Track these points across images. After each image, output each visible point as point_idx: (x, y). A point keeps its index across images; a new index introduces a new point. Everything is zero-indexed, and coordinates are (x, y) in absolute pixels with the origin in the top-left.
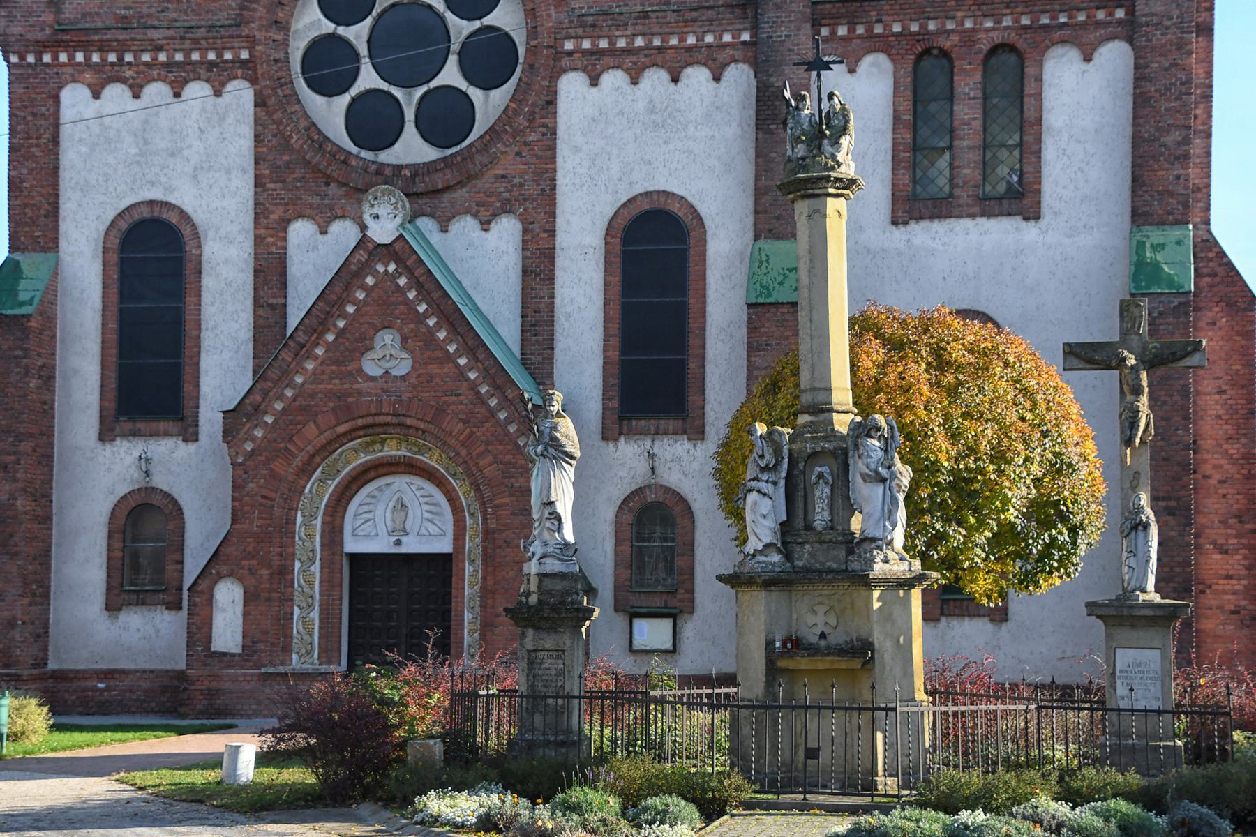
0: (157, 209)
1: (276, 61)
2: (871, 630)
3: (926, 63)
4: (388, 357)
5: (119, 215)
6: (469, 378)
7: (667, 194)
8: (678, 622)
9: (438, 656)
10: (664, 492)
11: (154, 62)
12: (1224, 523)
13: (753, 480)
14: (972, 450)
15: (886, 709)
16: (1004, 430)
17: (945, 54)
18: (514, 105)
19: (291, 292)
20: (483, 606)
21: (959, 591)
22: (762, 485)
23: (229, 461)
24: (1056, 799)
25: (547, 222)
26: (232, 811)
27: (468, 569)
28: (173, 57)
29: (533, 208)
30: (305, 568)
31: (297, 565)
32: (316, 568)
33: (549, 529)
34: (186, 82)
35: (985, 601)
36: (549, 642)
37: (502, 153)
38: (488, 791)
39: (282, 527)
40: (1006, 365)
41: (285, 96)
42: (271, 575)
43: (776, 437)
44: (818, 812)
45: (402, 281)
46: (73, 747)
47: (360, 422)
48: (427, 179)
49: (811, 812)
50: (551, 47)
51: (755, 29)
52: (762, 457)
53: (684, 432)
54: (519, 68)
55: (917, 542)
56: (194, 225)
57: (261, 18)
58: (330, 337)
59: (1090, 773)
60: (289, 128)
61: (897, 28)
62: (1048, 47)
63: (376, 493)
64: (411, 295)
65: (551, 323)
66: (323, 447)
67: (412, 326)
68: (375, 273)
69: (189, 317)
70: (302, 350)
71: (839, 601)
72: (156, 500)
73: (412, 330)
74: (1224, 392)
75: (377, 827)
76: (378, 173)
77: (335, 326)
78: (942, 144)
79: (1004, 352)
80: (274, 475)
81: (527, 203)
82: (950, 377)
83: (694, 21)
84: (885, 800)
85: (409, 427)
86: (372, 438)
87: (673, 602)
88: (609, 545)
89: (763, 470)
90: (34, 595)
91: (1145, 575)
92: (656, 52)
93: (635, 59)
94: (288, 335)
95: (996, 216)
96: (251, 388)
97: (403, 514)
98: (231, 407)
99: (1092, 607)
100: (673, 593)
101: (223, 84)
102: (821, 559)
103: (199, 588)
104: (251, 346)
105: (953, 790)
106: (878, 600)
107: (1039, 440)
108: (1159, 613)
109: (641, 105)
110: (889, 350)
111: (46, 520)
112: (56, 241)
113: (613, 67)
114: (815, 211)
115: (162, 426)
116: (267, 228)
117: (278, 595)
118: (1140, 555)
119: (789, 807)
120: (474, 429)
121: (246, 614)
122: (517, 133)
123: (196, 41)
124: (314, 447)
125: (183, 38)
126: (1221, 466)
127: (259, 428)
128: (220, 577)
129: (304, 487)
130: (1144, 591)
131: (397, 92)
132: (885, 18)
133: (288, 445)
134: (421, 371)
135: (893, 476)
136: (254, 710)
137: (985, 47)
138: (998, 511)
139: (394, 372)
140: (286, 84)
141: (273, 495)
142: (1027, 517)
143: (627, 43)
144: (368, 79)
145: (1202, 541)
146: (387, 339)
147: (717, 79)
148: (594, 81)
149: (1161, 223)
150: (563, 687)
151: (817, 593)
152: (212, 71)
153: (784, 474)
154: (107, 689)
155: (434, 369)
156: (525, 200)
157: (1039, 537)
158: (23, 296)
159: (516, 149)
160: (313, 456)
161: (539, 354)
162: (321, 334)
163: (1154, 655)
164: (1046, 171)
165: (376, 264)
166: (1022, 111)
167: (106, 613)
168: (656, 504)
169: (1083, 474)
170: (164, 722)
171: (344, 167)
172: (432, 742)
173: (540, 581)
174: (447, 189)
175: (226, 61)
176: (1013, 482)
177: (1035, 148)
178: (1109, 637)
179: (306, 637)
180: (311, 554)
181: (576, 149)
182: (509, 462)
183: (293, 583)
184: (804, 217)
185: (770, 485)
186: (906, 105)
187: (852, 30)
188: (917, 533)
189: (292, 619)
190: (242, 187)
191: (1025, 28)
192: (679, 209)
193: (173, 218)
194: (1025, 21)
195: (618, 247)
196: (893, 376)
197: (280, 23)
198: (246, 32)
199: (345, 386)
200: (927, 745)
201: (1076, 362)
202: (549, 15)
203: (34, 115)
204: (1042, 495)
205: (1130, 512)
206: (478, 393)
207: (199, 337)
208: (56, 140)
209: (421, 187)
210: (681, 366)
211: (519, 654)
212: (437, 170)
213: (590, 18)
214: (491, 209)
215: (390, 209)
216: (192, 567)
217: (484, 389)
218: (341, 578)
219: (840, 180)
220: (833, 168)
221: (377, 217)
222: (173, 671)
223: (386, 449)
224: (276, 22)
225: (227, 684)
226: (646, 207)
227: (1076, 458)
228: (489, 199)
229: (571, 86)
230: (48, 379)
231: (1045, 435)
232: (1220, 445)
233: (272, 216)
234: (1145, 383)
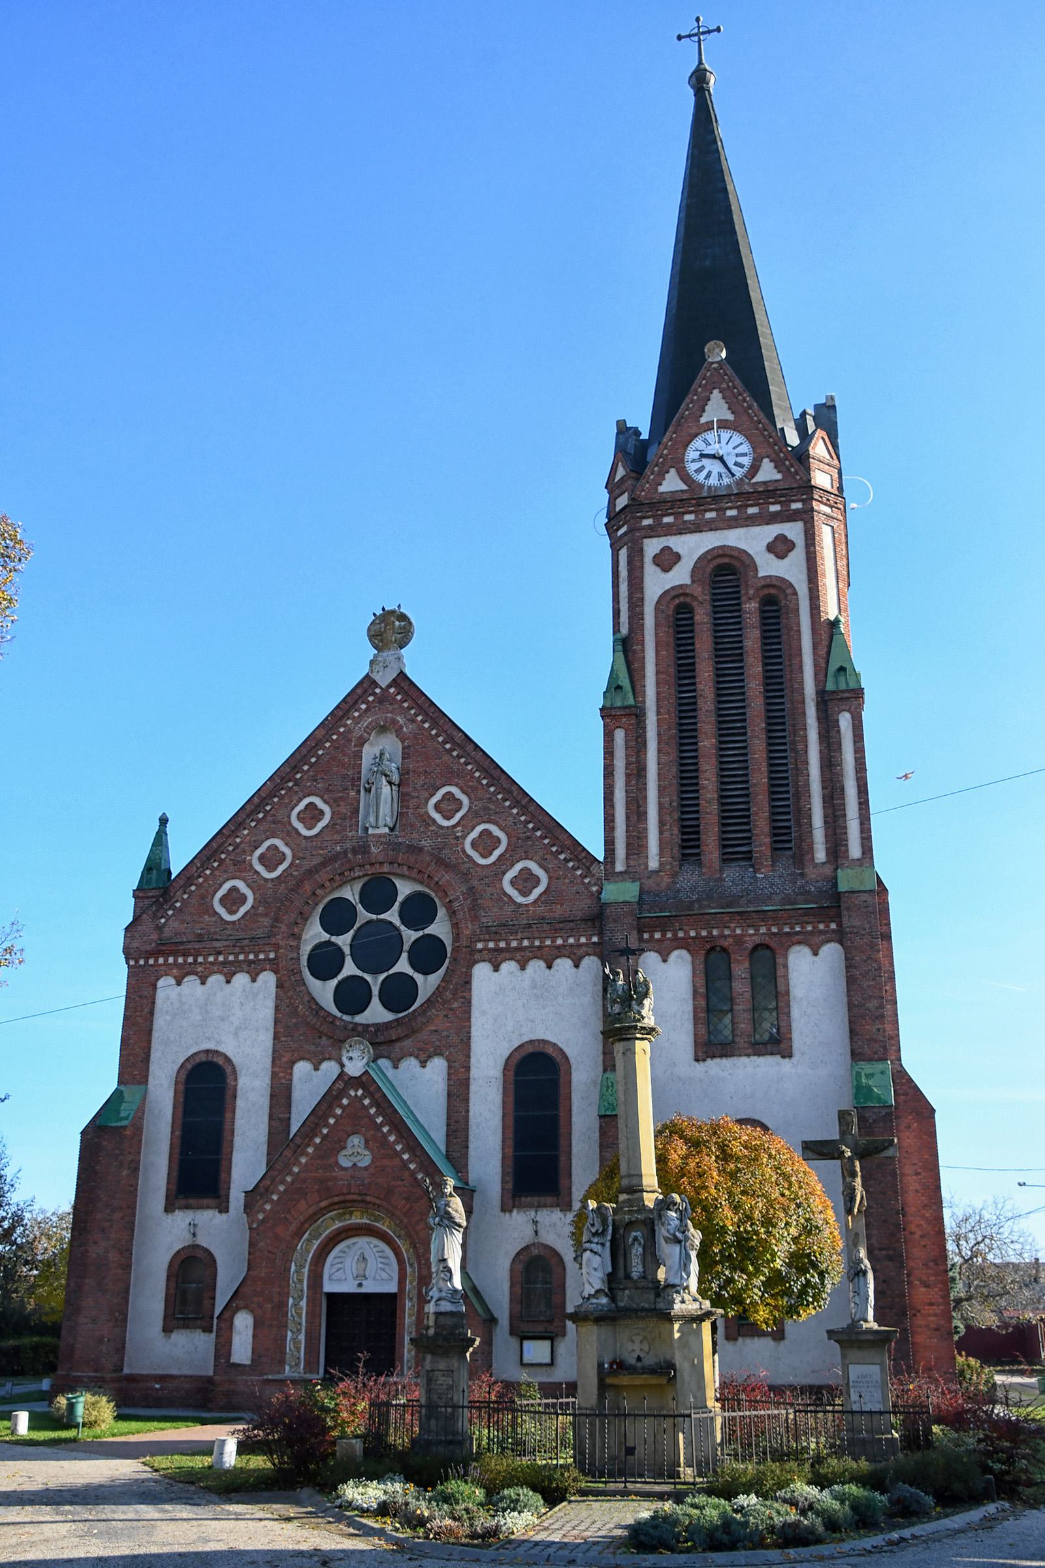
0: (210, 1055)
1: (292, 959)
2: (674, 1353)
3: (713, 955)
5: (187, 1059)
9: (366, 1374)
12: (925, 1265)
13: (588, 1242)
14: (749, 1218)
15: (684, 1416)
16: (770, 1203)
17: (724, 950)
19: (294, 1109)
21: (746, 1318)
22: (593, 1246)
23: (247, 1226)
24: (809, 1483)
26: (212, 1492)
27: (408, 1304)
31: (291, 1301)
32: (303, 1303)
33: (443, 1279)
34: (235, 973)
35: (764, 1326)
36: (442, 1365)
37: (436, 1016)
38: (393, 1480)
40: (770, 1156)
43: (603, 1211)
44: (634, 1498)
46: (128, 1433)
47: (336, 1199)
49: (630, 1498)
51: (601, 934)
52: (593, 1225)
53: (558, 1206)
54: (447, 961)
55: (713, 1285)
58: (318, 1140)
59: (833, 1462)
61: (692, 933)
62: (790, 946)
63: (346, 1250)
64: (373, 1111)
65: (466, 1130)
66: (311, 1217)
69: (227, 1127)
70: (299, 1150)
71: (651, 1332)
72: (199, 1254)
74: (919, 1173)
75: (309, 1509)
76: (353, 1029)
77: (321, 1132)
78: (726, 1008)
79: (768, 1148)
82: (732, 1166)
83: (561, 929)
84: (685, 1487)
85: (370, 1202)
88: (506, 1286)
89: (594, 1234)
90: (117, 1320)
91: (867, 1309)
93: (523, 954)
94: (291, 1136)
95: (763, 1055)
97: (363, 1265)
98: (251, 1189)
99: (831, 1333)
100: (550, 1321)
101: (257, 974)
102: (638, 1301)
104: (266, 1146)
105: (734, 1479)
106: (678, 1331)
107: (795, 1210)
108: (878, 1337)
109: (527, 983)
110: (690, 1147)
111: (128, 1267)
112: (146, 1077)
114: (627, 1050)
115: (206, 1201)
116: (280, 1067)
118: (862, 1294)
119: (613, 1493)
121: (254, 1336)
123: (242, 948)
125: (234, 946)
126: (921, 1225)
128: (238, 1309)
130: (866, 1321)
131: (368, 977)
132: (685, 928)
135: (687, 1238)
137: (750, 946)
138: (768, 1262)
139: (360, 1165)
142: (789, 1265)
144: (349, 969)
145: (912, 1278)
146: (356, 1141)
147: (577, 966)
148: (496, 968)
149: (870, 1060)
150: (452, 1399)
151: (635, 1326)
153: (609, 1238)
154: (162, 1389)
155: (386, 1162)
157: (798, 1280)
158: (123, 1114)
163: (877, 1368)
164: (794, 1026)
166: (776, 987)
167: (163, 1334)
168: (538, 1257)
169: (826, 1233)
170: (196, 1414)
172: (354, 1441)
173: (436, 1318)
174: (399, 1039)
175: (261, 960)
176: (778, 1240)
177: (786, 1010)
178: (844, 1356)
181: (484, 1013)
184: (620, 1054)
185: (599, 1246)
186: (701, 982)
187: (664, 935)
188: (712, 1278)
190: (266, 1039)
191: (774, 934)
194: (774, 930)
195: (512, 1078)
196: (693, 1165)
198: (273, 941)
200: (719, 1441)
201: (810, 1154)
202: (467, 927)
203: (140, 997)
204: (799, 1249)
205: (853, 1263)
207: (232, 1141)
208: (152, 1013)
209: (381, 1039)
210: (555, 1160)
211: (421, 1374)
216: (221, 1300)
218: (321, 1311)
219: (643, 1028)
220: (639, 1021)
221: (351, 1058)
222: (205, 1377)
227: (821, 1222)
229: (481, 972)
230: (135, 1168)
231: (798, 1206)
232: (919, 1211)
234: (858, 1169)
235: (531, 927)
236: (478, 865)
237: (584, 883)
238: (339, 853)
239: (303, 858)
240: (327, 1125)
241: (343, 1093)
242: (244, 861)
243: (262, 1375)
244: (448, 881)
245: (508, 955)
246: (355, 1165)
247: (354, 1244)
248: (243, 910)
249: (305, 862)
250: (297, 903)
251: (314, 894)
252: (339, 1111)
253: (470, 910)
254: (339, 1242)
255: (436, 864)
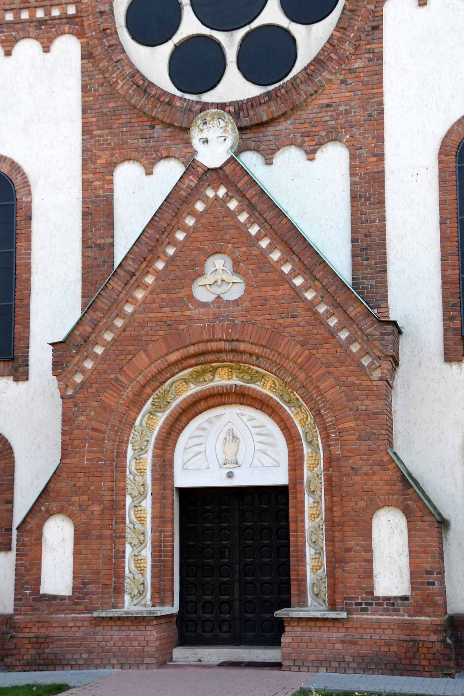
1: (101, 13)
4: (219, 282)
6: (306, 299)
20: (330, 541)
25: (375, 146)
27: (308, 501)
30: (136, 503)
31: (129, 500)
32: (147, 504)
34: (16, 40)
39: (113, 461)
41: (110, 46)
42: (102, 511)
45: (233, 205)
47: (192, 350)
48: (252, 113)
58: (160, 265)
60: (114, 75)
63: (206, 425)
64: (243, 218)
65: (383, 245)
66: (154, 377)
67: (245, 249)
68: (205, 199)
73: (245, 253)
77: (165, 253)
80: (104, 407)
81: (354, 129)
85: (244, 352)
86: (203, 367)
96: (81, 319)
97: (234, 445)
117: (109, 532)
120: (314, 351)
121: (76, 553)
122: (343, 59)
124: (144, 377)
128: (49, 514)
129: (135, 419)
136: (85, 660)
139: (227, 297)
140: (111, 35)
141: (103, 427)
152: (41, 29)
155: (268, 291)
156: (351, 126)
159: (342, 77)
160: (144, 386)
161: (372, 278)
162: (151, 263)
171: (169, 108)
174: (272, 121)
175: (54, 18)
179: (138, 577)
180: (142, 489)
182: (354, 384)
189: (124, 557)
195: (454, 165)
199: (176, 314)
206: (316, 313)
214: (316, 138)
215: (219, 132)
217: (322, 309)
221: (206, 141)
223: (217, 378)
225: (57, 630)
228: (314, 129)
233: (99, 161)
240: (173, 242)
243: (90, 611)
246: (219, 297)
247: (218, 416)
252: (190, 221)
254: (197, 414)
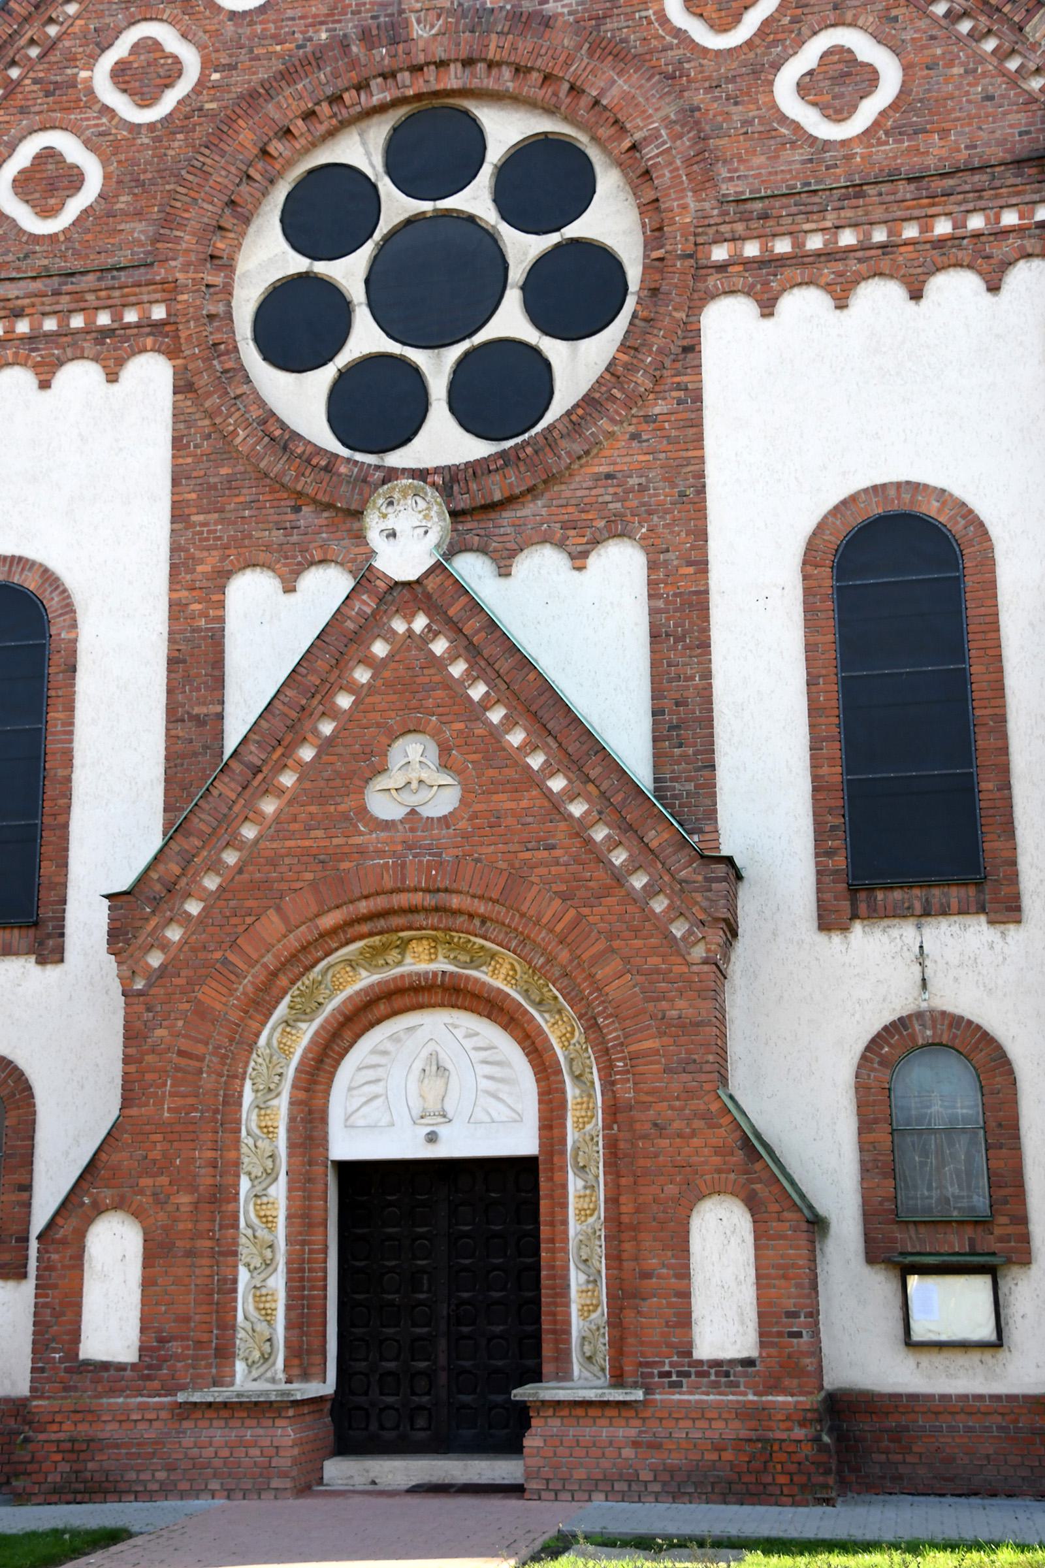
1: (211, 317)
4: (414, 785)
6: (571, 815)
7: (915, 487)
8: (1001, 1282)
10: (950, 1026)
11: (9, 336)
18: (625, 358)
20: (615, 1258)
25: (693, 548)
27: (574, 1184)
28: (41, 326)
29: (666, 526)
31: (245, 1184)
32: (279, 1191)
34: (61, 363)
37: (611, 435)
39: (216, 1111)
41: (225, 372)
42: (196, 1205)
45: (440, 647)
47: (363, 907)
48: (474, 486)
50: (690, 256)
53: (981, 909)
56: (65, 591)
57: (187, 251)
58: (307, 753)
60: (231, 421)
63: (389, 1046)
64: (458, 669)
65: (708, 721)
66: (294, 957)
68: (389, 636)
69: (53, 745)
77: (316, 732)
80: (202, 1012)
81: (655, 518)
86: (384, 938)
87: (989, 1242)
92: (880, 252)
93: (840, 266)
94: (228, 752)
96: (161, 850)
97: (440, 1083)
103: (60, 1234)
113: (800, 284)
120: (585, 911)
121: (147, 1283)
123: (78, 296)
124: (276, 957)
125: (57, 293)
127: (174, 926)
128: (98, 1210)
133: (228, 954)
134: (477, 807)
136: (162, 1483)
139: (427, 812)
140: (227, 352)
141: (200, 1049)
143: (826, 243)
148: (767, 308)
152: (104, 344)
155: (503, 801)
156: (650, 513)
159: (632, 429)
160: (274, 974)
161: (688, 780)
162: (290, 749)
165: (390, 619)
171: (327, 477)
174: (510, 501)
175: (128, 326)
179: (261, 1327)
180: (269, 1163)
183: (237, 1219)
189: (235, 1290)
192: (939, 511)
193: (31, 583)
197: (220, 258)
198: (160, 273)
199: (335, 841)
202: (684, 207)
206: (589, 841)
212: (490, 471)
213: (758, 205)
214: (588, 532)
215: (416, 519)
217: (600, 834)
218: (326, 1210)
221: (393, 534)
223: (409, 959)
224: (212, 257)
225: (109, 1427)
226: (877, 510)
228: (584, 516)
233: (199, 568)
235: (860, 195)
236: (705, 50)
237: (1004, 73)
238: (327, 46)
239: (232, 67)
240: (331, 712)
241: (372, 626)
242: (72, 83)
243: (171, 1392)
244: (625, 96)
245: (798, 274)
246: (413, 812)
247: (410, 1029)
248: (74, 207)
249: (236, 77)
250: (218, 177)
251: (264, 152)
253: (689, 162)
255: (591, 53)
